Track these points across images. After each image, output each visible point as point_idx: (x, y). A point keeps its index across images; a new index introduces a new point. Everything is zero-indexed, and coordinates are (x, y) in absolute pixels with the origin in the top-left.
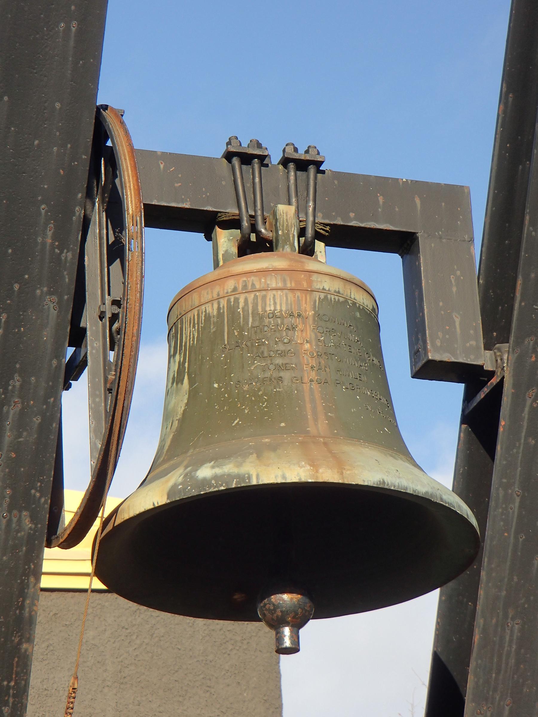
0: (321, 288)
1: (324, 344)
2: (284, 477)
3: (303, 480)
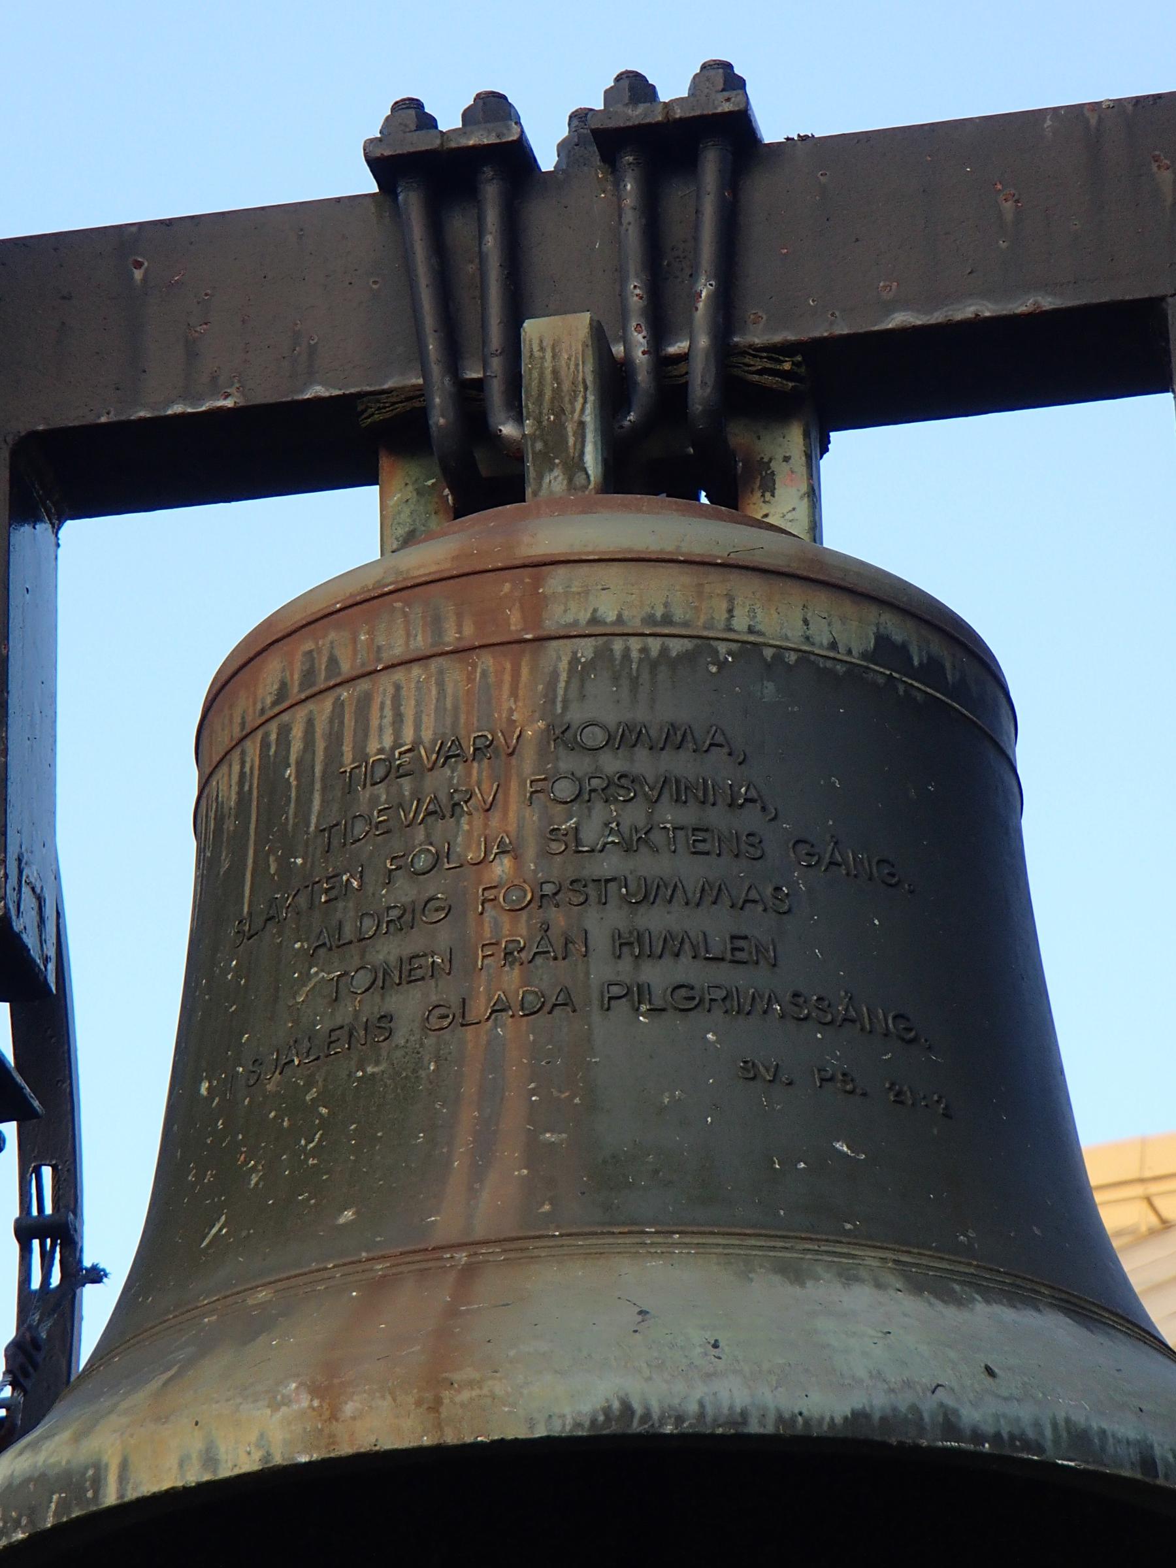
0: (584, 616)
1: (573, 846)
2: (210, 1459)
3: (278, 1460)
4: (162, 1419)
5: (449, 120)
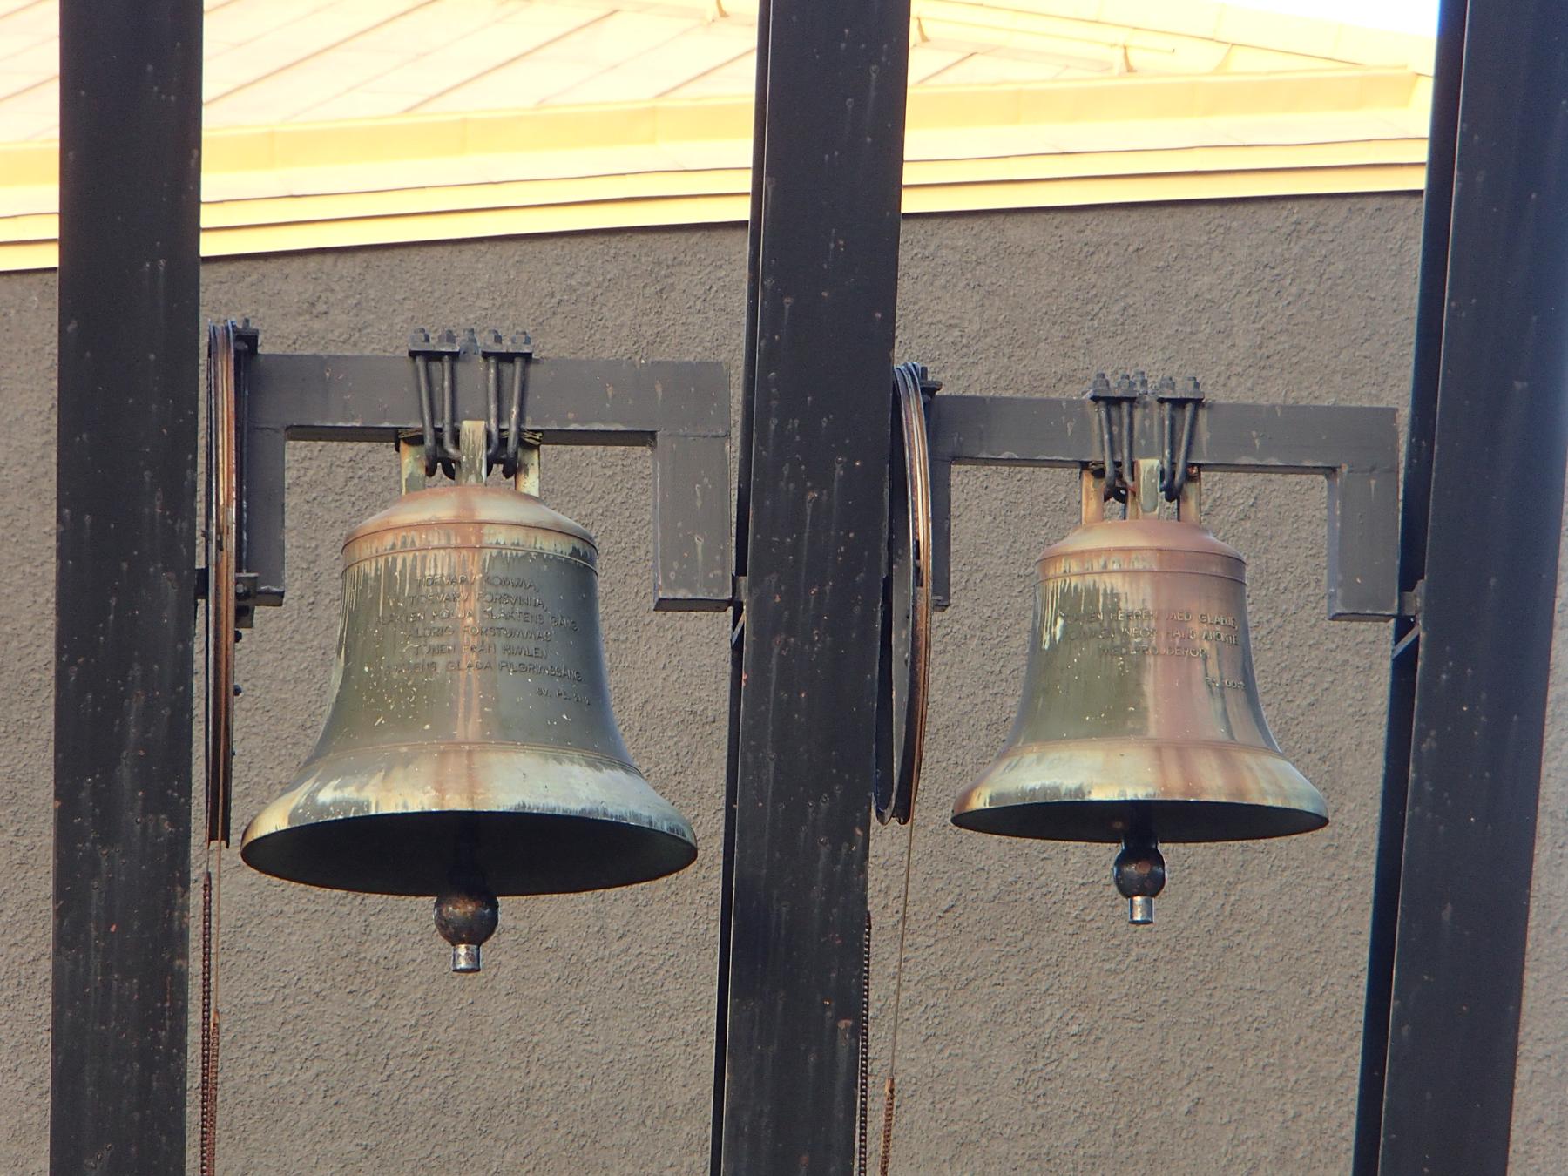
2: (405, 806)
3: (427, 809)
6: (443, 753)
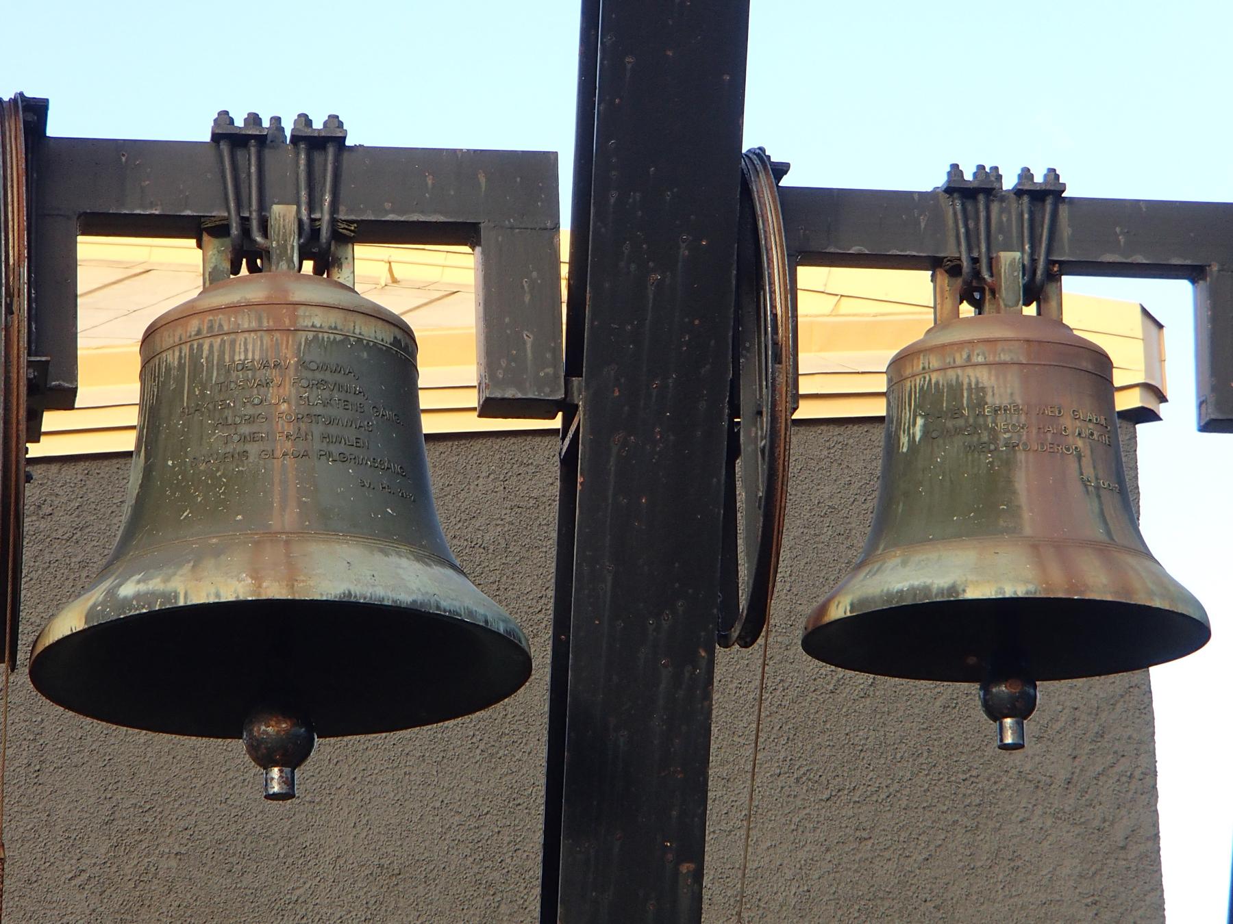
2: (218, 595)
3: (241, 598)
4: (199, 580)
5: (239, 122)
6: (257, 543)
